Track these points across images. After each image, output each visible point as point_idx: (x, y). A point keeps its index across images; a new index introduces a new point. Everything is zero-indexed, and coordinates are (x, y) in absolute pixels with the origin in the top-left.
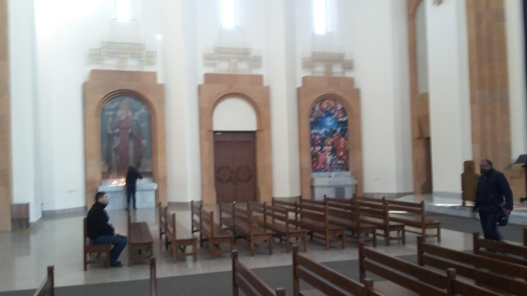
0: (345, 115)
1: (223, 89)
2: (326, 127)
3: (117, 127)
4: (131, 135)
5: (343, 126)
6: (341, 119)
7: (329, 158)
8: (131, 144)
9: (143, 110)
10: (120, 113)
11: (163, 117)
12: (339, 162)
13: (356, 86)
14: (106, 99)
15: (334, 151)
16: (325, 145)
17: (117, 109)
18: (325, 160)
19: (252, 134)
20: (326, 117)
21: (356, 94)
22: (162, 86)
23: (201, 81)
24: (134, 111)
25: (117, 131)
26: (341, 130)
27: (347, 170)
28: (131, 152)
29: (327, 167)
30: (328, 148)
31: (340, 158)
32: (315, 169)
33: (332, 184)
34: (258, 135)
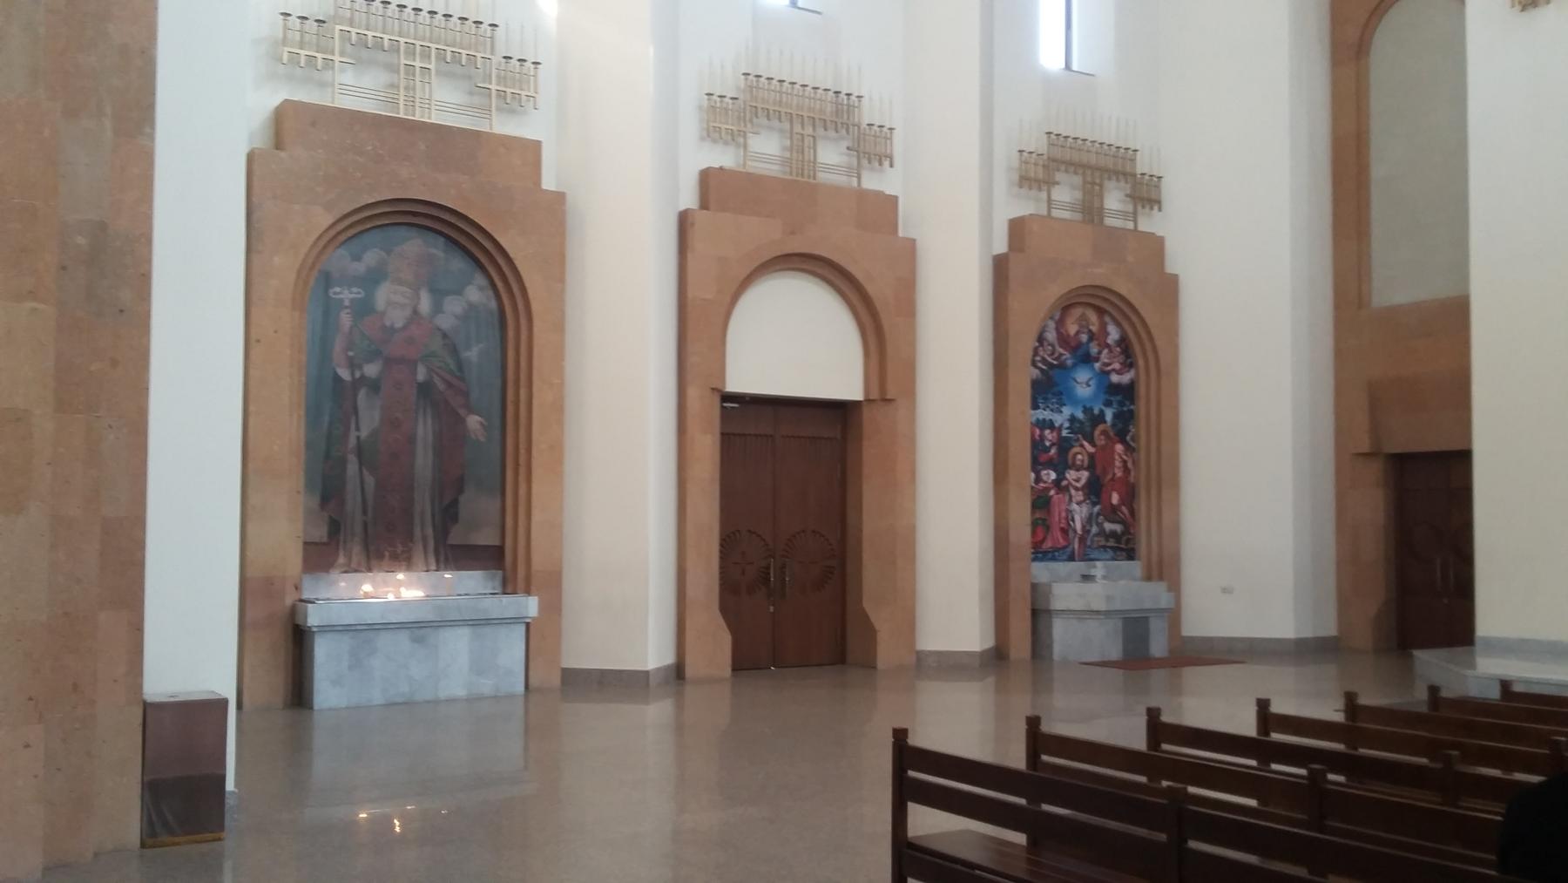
0: (1129, 364)
1: (767, 234)
2: (1075, 401)
3: (374, 355)
4: (425, 389)
5: (1121, 404)
6: (1115, 378)
7: (1080, 513)
8: (424, 430)
9: (476, 293)
10: (384, 294)
11: (559, 327)
12: (1108, 526)
13: (1171, 267)
14: (339, 233)
15: (1094, 490)
16: (1068, 467)
17: (373, 279)
18: (1070, 518)
19: (839, 412)
20: (1075, 365)
21: (1168, 290)
22: (560, 197)
23: (688, 198)
24: (438, 294)
25: (371, 370)
26: (1116, 416)
27: (1131, 555)
28: (424, 462)
29: (1071, 547)
30: (1077, 477)
31: (1112, 513)
32: (1040, 553)
33: (1118, 606)
34: (866, 413)
